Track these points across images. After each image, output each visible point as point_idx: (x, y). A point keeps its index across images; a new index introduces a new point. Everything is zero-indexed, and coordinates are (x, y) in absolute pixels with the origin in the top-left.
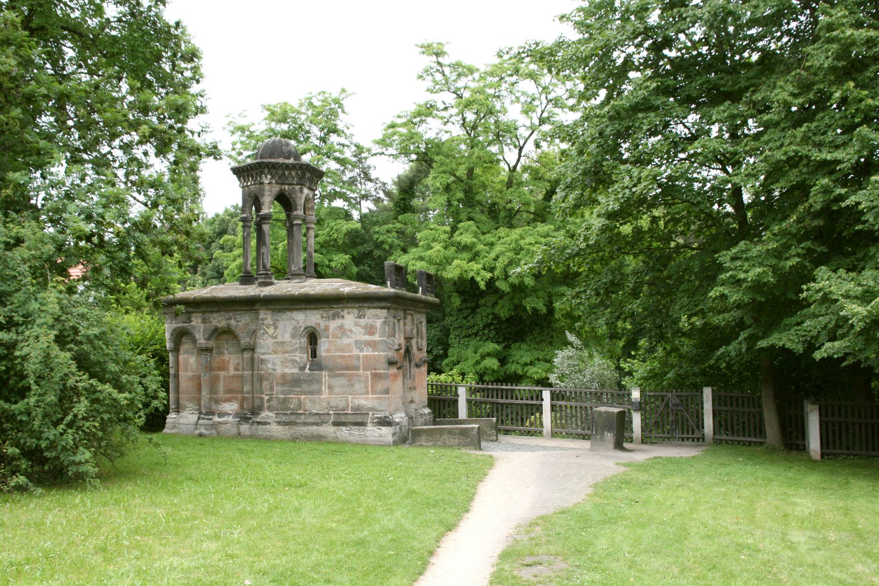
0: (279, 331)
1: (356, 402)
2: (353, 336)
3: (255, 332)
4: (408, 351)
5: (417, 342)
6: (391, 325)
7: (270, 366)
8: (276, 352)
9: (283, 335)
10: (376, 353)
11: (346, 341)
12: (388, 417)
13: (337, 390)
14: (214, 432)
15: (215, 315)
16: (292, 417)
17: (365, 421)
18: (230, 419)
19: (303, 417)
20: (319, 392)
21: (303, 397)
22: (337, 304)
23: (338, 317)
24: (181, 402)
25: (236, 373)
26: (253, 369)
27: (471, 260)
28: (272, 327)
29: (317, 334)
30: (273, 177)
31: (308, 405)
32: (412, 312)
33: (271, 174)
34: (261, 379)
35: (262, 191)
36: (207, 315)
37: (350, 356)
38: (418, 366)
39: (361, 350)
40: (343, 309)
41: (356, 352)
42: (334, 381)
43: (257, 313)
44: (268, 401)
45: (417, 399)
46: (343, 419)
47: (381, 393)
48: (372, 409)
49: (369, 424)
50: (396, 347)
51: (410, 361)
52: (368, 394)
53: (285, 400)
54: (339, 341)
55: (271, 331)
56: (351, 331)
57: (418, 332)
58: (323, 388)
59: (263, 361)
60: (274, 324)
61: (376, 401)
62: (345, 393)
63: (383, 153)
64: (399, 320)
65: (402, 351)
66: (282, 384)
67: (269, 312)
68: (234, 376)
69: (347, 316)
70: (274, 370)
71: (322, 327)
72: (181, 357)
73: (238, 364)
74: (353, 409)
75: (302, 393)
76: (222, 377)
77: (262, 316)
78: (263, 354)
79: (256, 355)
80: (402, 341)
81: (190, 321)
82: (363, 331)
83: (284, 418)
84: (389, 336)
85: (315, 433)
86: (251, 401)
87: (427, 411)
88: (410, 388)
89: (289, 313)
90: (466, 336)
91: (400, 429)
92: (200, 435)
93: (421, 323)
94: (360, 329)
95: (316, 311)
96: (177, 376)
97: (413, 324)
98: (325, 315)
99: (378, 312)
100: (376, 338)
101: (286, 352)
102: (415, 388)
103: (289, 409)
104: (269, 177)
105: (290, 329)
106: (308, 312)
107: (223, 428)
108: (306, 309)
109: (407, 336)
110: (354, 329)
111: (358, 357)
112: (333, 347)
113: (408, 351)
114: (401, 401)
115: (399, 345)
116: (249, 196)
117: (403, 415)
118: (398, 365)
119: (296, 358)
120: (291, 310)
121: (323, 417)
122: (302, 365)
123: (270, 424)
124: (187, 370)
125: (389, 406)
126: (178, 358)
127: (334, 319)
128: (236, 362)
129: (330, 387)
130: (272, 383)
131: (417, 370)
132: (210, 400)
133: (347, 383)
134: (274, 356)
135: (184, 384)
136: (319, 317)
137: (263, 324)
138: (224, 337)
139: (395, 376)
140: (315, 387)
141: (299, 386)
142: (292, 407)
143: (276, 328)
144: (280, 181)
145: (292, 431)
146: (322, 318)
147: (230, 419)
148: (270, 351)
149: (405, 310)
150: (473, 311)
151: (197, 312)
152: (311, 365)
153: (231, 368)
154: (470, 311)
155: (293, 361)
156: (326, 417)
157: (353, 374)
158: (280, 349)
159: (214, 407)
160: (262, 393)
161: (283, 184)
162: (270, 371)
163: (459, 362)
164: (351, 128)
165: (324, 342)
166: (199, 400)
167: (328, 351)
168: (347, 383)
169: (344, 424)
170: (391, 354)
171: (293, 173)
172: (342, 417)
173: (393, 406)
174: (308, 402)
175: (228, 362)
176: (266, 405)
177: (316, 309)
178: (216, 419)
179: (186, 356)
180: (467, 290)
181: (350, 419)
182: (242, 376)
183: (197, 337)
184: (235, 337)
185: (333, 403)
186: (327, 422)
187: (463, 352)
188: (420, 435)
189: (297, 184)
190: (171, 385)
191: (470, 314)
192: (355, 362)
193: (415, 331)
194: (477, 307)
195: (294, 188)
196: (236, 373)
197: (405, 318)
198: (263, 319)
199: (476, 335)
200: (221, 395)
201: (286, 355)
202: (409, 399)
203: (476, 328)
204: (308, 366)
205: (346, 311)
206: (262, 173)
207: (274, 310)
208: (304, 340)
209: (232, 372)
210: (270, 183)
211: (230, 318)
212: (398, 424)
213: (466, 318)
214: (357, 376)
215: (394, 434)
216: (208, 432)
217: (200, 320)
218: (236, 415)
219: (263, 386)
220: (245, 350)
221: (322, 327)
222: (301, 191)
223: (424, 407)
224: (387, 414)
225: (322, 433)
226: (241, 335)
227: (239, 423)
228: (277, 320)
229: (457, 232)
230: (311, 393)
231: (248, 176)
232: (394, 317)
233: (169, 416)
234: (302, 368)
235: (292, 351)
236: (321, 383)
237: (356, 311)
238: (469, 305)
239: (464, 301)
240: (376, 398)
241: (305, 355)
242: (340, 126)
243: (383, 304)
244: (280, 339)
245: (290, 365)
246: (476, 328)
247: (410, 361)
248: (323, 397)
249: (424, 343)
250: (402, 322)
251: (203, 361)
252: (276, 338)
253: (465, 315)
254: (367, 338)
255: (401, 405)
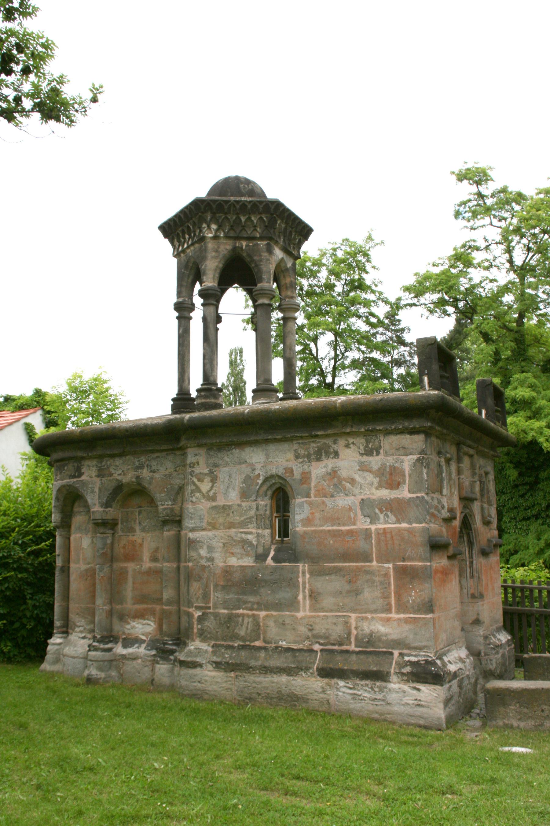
0: (220, 486)
1: (367, 628)
2: (357, 491)
3: (181, 489)
4: (466, 524)
5: (482, 508)
6: (433, 466)
7: (203, 552)
8: (213, 526)
9: (226, 494)
10: (404, 525)
11: (342, 501)
12: (433, 663)
13: (328, 601)
14: (114, 673)
15: (118, 461)
16: (243, 653)
17: (384, 669)
18: (142, 650)
19: (263, 654)
20: (293, 604)
21: (262, 614)
22: (324, 428)
23: (328, 454)
24: (71, 615)
25: (153, 565)
26: (179, 560)
27: (530, 418)
28: (207, 479)
29: (288, 489)
30: (220, 227)
31: (273, 631)
32: (471, 452)
33: (217, 222)
34: (189, 577)
35: (203, 252)
36: (108, 462)
37: (350, 532)
38: (485, 553)
39: (374, 519)
40: (336, 436)
41: (363, 523)
42: (322, 584)
43: (185, 455)
44: (201, 619)
45: (485, 616)
46: (339, 663)
47: (418, 611)
48: (399, 644)
49: (394, 678)
50: (445, 514)
51: (471, 544)
52: (389, 611)
53: (230, 618)
54: (329, 502)
55: (205, 486)
56: (352, 481)
57: (482, 490)
58: (300, 597)
59: (192, 543)
60: (211, 472)
61: (406, 627)
62: (341, 609)
63: (414, 305)
64: (448, 461)
65: (457, 523)
66: (224, 587)
67: (202, 451)
68: (149, 572)
69: (344, 453)
70: (211, 559)
71: (297, 474)
72: (73, 537)
73: (157, 550)
74: (359, 642)
75: (261, 606)
76: (130, 573)
77: (190, 459)
78: (193, 530)
79: (183, 533)
80: (456, 503)
81: (81, 474)
82: (376, 481)
83: (228, 656)
84: (430, 490)
85: (285, 690)
86: (174, 618)
87: (504, 637)
88: (473, 596)
89: (236, 452)
90: (524, 519)
91: (460, 686)
92: (89, 681)
93: (487, 474)
94: (370, 477)
95: (286, 446)
96: (66, 570)
97: (474, 474)
98: (302, 452)
99: (406, 440)
100: (404, 493)
101: (231, 526)
102: (481, 596)
103: (236, 637)
104: (214, 227)
105: (238, 482)
106: (272, 447)
107: (129, 667)
108: (267, 441)
109: (464, 494)
110: (357, 478)
111: (367, 534)
112: (317, 515)
113: (466, 524)
114: (457, 624)
115: (451, 510)
116: (186, 266)
117: (463, 653)
118: (451, 551)
119: (250, 537)
120: (241, 445)
121: (300, 657)
122: (260, 550)
123: (200, 665)
124: (78, 562)
125: (436, 637)
126: (69, 539)
127: (319, 459)
128: (153, 545)
129: (314, 596)
130: (207, 586)
131: (482, 560)
132: (110, 613)
133: (347, 587)
134: (210, 534)
135: (75, 585)
136: (290, 455)
137: (192, 473)
138: (136, 501)
139: (445, 572)
140: (283, 595)
141: (255, 593)
142: (242, 633)
143: (214, 480)
144: (232, 234)
145: (241, 683)
146: (297, 457)
147: (142, 650)
148: (204, 524)
149: (458, 445)
150: (533, 486)
151: (90, 458)
152: (277, 551)
153: (146, 556)
154: (527, 487)
155: (245, 543)
156: (307, 657)
157: (359, 569)
158: (221, 520)
159: (117, 627)
160: (190, 604)
161: (238, 238)
162: (203, 562)
163: (516, 552)
164: (379, 285)
165: (301, 505)
166: (93, 615)
167: (308, 521)
168: (347, 587)
169: (341, 674)
170: (435, 527)
171: (254, 219)
172: (339, 658)
173: (443, 636)
174: (271, 624)
175: (141, 545)
176: (196, 627)
177: (285, 440)
178: (119, 650)
179: (78, 535)
180: (523, 460)
181: (354, 663)
182: (158, 572)
183: (90, 501)
184: (152, 501)
185: (320, 628)
186: (307, 669)
187: (521, 539)
188: (504, 704)
189: (262, 238)
190: (56, 586)
191: (528, 491)
192: (362, 544)
193: (477, 488)
194: (537, 482)
195: (257, 245)
196: (153, 565)
197: (459, 460)
198: (192, 465)
199: (537, 517)
200: (129, 605)
201: (232, 531)
202: (472, 617)
203: (537, 508)
204: (272, 553)
205: (342, 442)
206: (202, 220)
207: (209, 447)
208: (265, 502)
209: (147, 564)
210: (216, 237)
211: (141, 467)
212: (455, 675)
213: (522, 496)
214: (367, 572)
215: (447, 702)
216: (103, 675)
217: (94, 472)
218: (153, 644)
219: (192, 590)
220: (165, 523)
221: (297, 474)
222: (270, 251)
223: (498, 630)
224: (432, 656)
225: (298, 692)
226: (158, 496)
227: (154, 662)
228: (216, 465)
229: (510, 387)
230: (278, 606)
231: (183, 233)
232: (439, 453)
233: (51, 641)
234: (261, 557)
235: (243, 524)
236: (296, 586)
237: (361, 441)
238: (527, 479)
239: (520, 474)
240: (407, 621)
241: (267, 532)
242: (368, 280)
243: (415, 424)
244: (221, 501)
245: (237, 550)
246: (537, 508)
247: (471, 544)
248: (300, 615)
249: (493, 512)
250: (453, 466)
251: (99, 544)
252: (214, 499)
253: (521, 493)
254: (385, 493)
255: (458, 632)
